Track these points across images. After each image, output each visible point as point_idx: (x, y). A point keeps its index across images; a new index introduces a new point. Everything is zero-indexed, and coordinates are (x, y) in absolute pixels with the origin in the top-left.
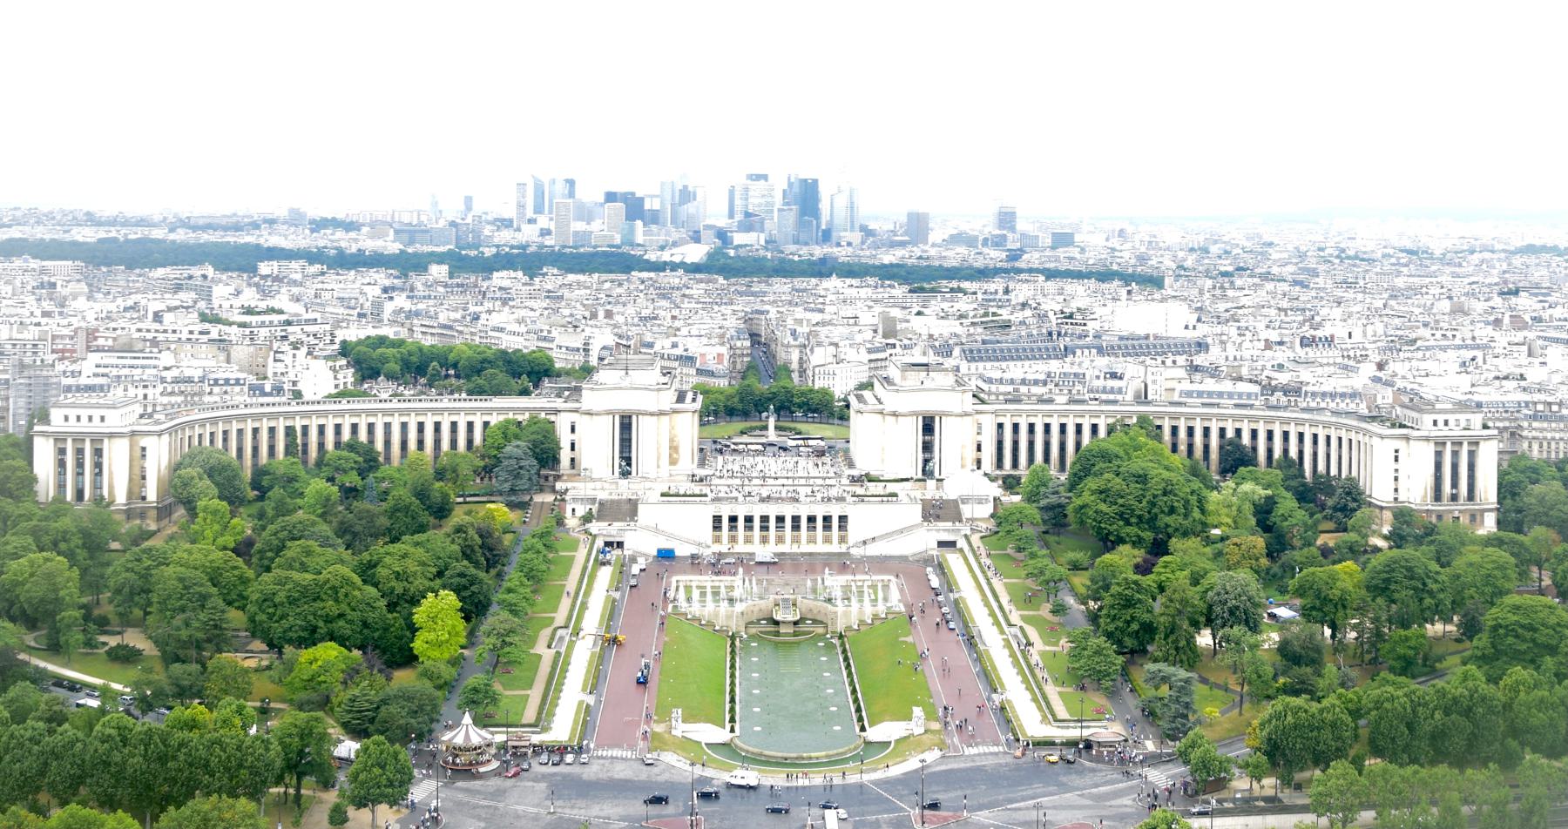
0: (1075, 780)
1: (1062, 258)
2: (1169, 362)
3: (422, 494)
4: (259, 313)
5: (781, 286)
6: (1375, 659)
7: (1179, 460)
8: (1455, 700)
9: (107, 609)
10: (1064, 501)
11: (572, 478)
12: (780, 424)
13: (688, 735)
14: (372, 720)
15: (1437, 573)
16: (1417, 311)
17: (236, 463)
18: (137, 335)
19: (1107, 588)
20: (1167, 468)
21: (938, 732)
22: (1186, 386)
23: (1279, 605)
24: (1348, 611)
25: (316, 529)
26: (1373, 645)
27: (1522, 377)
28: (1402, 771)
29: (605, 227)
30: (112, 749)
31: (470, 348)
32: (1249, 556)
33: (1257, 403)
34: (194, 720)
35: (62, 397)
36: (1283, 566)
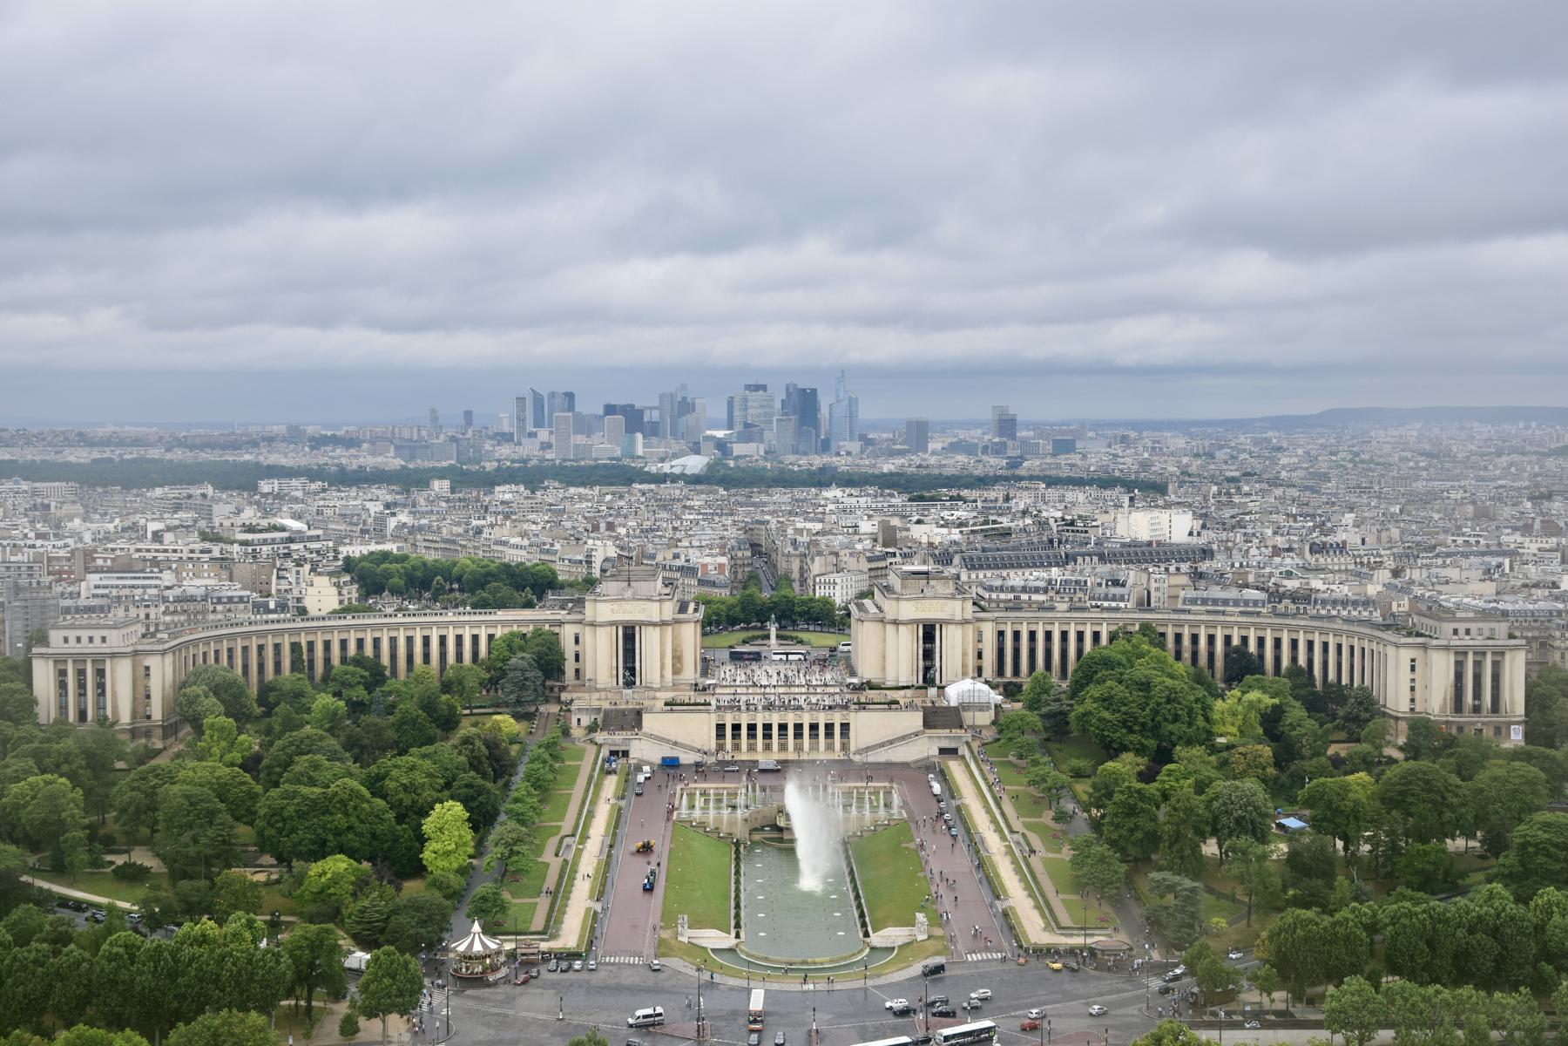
0: (1077, 987)
1: (1065, 464)
2: (1172, 569)
3: (428, 706)
4: (261, 531)
5: (780, 496)
7: (1181, 668)
9: (113, 827)
11: (577, 688)
12: (783, 633)
13: (693, 941)
15: (1458, 787)
16: (1436, 516)
17: (241, 680)
18: (136, 555)
19: (1109, 795)
20: (1171, 676)
22: (1191, 594)
23: (1288, 816)
24: (1361, 823)
25: (324, 744)
26: (1389, 858)
27: (1555, 585)
28: (1422, 990)
29: (605, 440)
31: (474, 562)
32: (1253, 766)
33: (1264, 611)
34: (204, 935)
35: (61, 618)
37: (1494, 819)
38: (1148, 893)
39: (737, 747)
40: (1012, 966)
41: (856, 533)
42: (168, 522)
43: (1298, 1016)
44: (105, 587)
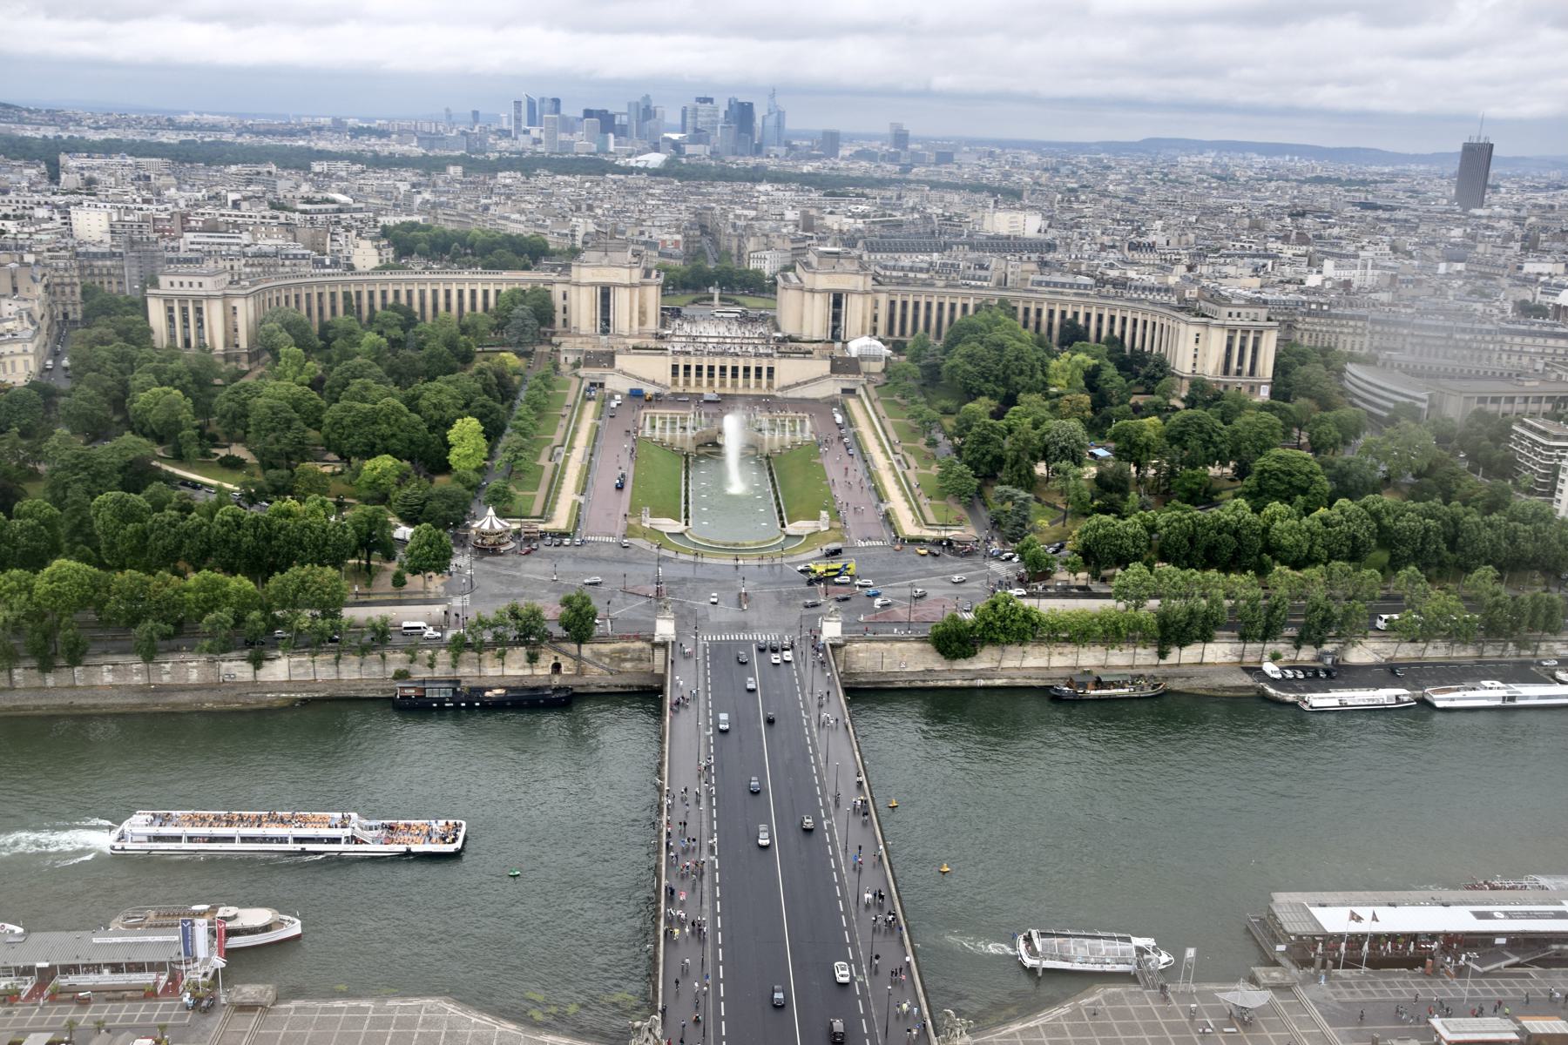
1: (944, 173)
2: (1025, 258)
3: (451, 344)
4: (316, 203)
5: (723, 188)
6: (1168, 490)
8: (1227, 524)
9: (215, 428)
10: (939, 361)
11: (568, 333)
14: (420, 512)
16: (1222, 226)
17: (307, 320)
18: (221, 219)
19: (969, 428)
20: (1020, 340)
21: (839, 529)
22: (1039, 278)
23: (1098, 447)
26: (1167, 480)
27: (1302, 282)
28: (1182, 573)
30: (229, 531)
31: (483, 232)
32: (1075, 411)
33: (1092, 293)
36: (1103, 418)
37: (1244, 454)
38: (991, 499)
39: (687, 383)
40: (891, 551)
41: (782, 220)
42: (244, 193)
43: (1095, 590)
44: (199, 243)
